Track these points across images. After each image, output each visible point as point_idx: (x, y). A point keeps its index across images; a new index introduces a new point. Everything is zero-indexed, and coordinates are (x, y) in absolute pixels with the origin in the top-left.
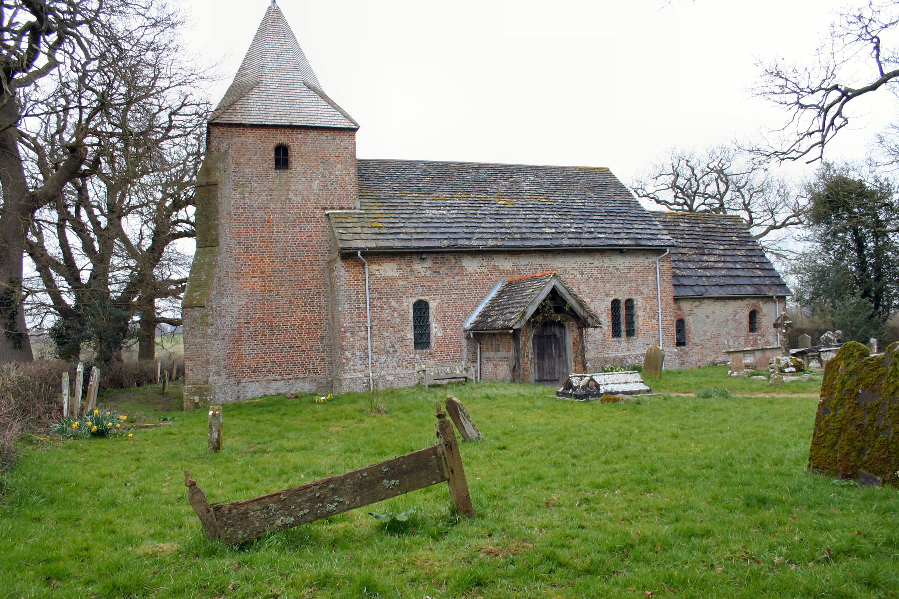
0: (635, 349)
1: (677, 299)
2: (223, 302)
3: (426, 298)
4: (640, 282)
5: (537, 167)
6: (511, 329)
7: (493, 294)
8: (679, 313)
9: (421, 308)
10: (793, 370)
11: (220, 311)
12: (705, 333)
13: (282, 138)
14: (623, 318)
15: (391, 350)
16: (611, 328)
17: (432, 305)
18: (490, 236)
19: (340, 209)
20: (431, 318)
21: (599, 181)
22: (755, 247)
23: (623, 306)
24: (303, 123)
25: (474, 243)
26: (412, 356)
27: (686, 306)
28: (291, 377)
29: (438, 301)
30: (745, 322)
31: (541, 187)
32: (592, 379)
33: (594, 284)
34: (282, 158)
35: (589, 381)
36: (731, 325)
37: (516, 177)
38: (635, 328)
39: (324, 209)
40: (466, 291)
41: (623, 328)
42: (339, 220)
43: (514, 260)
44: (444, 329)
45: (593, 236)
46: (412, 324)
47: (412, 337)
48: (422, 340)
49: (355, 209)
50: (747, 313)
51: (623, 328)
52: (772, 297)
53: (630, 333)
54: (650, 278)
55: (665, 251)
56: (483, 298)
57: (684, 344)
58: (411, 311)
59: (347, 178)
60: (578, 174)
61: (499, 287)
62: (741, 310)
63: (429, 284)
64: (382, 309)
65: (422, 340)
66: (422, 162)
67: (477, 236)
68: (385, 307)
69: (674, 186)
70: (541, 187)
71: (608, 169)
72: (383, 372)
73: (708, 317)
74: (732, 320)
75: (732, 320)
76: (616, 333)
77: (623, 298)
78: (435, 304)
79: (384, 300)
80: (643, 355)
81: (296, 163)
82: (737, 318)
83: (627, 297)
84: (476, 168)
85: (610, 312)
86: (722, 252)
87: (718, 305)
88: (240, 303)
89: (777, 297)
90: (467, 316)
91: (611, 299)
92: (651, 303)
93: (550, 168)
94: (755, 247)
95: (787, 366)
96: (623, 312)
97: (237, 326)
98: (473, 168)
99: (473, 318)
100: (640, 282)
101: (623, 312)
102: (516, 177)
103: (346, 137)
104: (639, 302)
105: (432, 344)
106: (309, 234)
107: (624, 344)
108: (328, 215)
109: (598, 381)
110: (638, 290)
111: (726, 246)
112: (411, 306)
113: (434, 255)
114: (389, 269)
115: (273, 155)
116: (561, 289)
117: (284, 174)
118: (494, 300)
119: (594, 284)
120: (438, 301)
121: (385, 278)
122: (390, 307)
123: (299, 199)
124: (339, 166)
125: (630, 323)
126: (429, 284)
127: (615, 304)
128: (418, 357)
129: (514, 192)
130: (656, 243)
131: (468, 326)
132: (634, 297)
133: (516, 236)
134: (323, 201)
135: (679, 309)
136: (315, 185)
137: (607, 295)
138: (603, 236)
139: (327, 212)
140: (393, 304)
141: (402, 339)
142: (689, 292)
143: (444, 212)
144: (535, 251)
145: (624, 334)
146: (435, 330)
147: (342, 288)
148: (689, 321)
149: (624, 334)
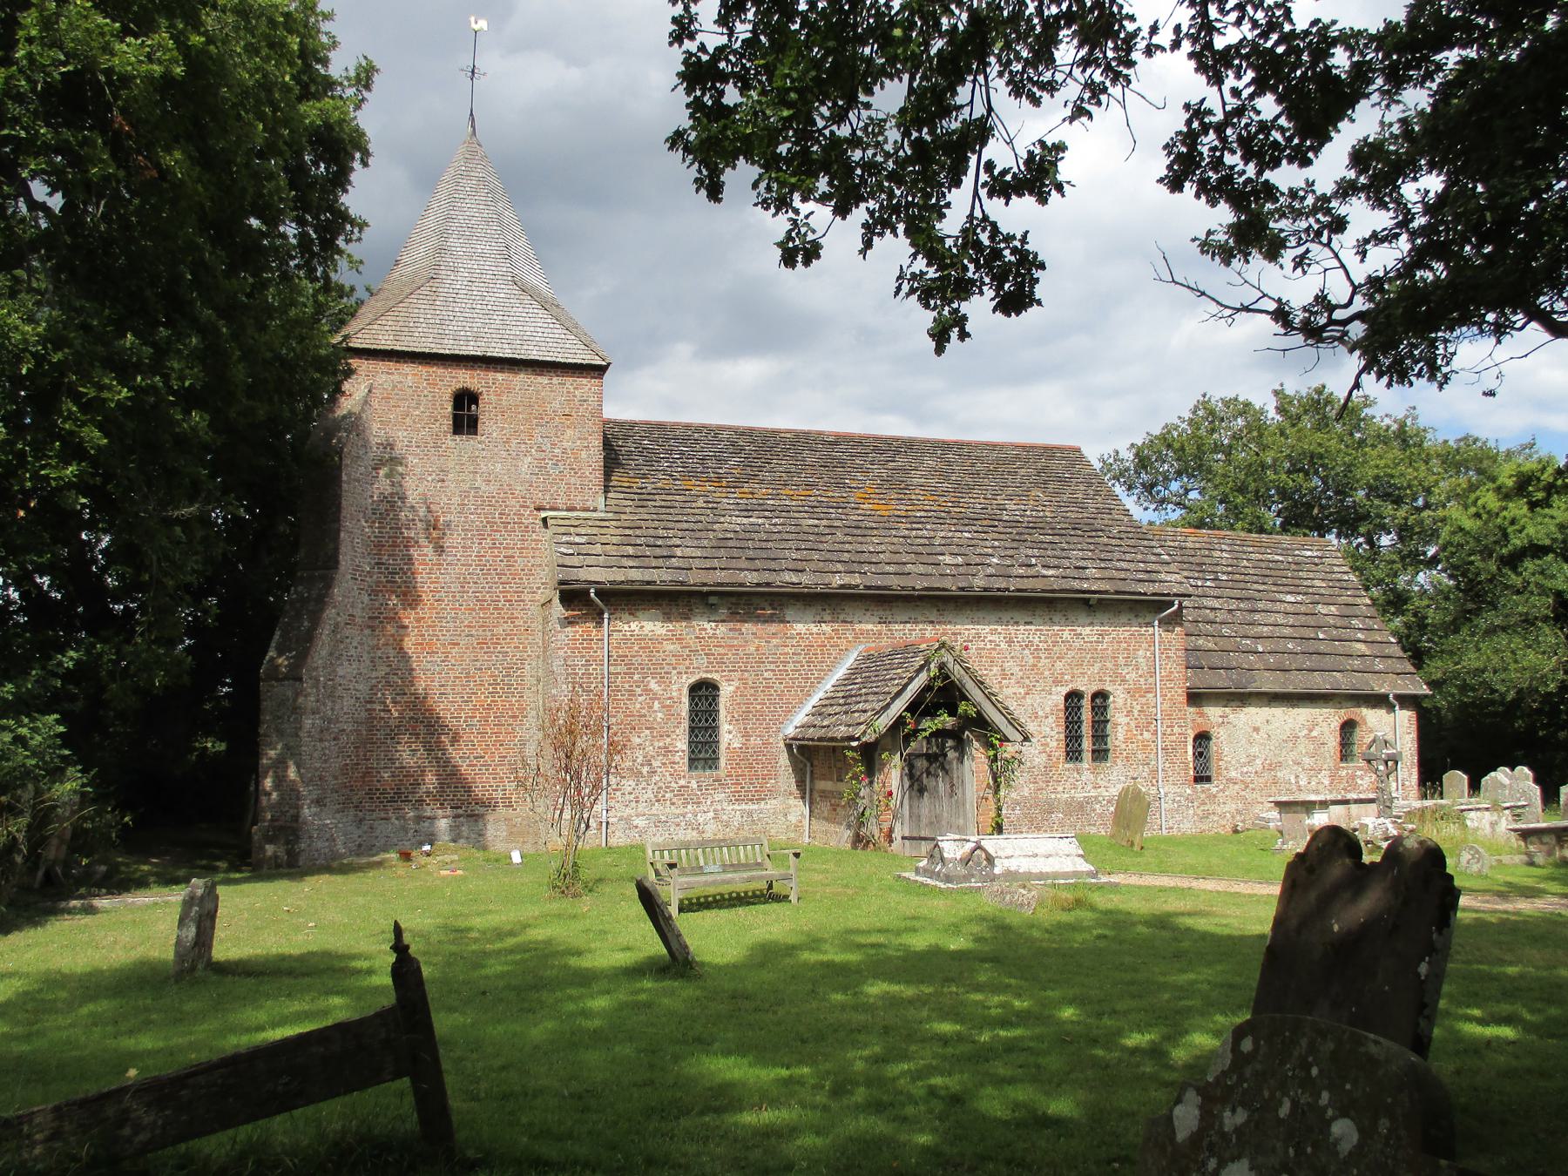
0: (1101, 785)
1: (1195, 698)
2: (340, 672)
4: (1121, 661)
5: (944, 442)
6: (858, 739)
7: (841, 672)
8: (1200, 720)
9: (703, 692)
11: (334, 687)
12: (1251, 760)
13: (466, 378)
14: (1086, 724)
15: (645, 770)
16: (1063, 744)
17: (726, 691)
18: (839, 567)
19: (568, 510)
20: (722, 713)
24: (506, 352)
25: (805, 579)
26: (682, 782)
27: (1214, 712)
28: (460, 811)
29: (736, 683)
30: (1333, 742)
32: (979, 847)
33: (1031, 661)
34: (465, 413)
38: (1110, 746)
39: (539, 509)
40: (790, 667)
41: (1087, 744)
42: (563, 530)
43: (881, 613)
44: (746, 735)
45: (1031, 572)
46: (686, 724)
47: (685, 747)
48: (703, 748)
49: (595, 510)
51: (1087, 744)
52: (1386, 697)
53: (1100, 754)
54: (1140, 653)
55: (1171, 604)
56: (820, 680)
57: (1208, 779)
58: (686, 700)
59: (584, 454)
60: (1017, 457)
61: (850, 661)
62: (1328, 720)
63: (721, 650)
64: (631, 693)
65: (703, 748)
66: (729, 428)
67: (813, 566)
68: (639, 691)
71: (1078, 450)
72: (628, 811)
73: (1256, 730)
74: (1307, 737)
75: (1307, 737)
76: (1073, 754)
77: (1088, 689)
78: (732, 688)
79: (636, 677)
81: (487, 424)
82: (1314, 734)
83: (1095, 688)
84: (830, 443)
85: (1062, 714)
86: (1290, 608)
88: (374, 674)
89: (1397, 697)
90: (789, 711)
91: (1065, 690)
92: (1143, 700)
96: (1086, 714)
97: (364, 714)
99: (800, 718)
100: (1121, 661)
101: (1086, 714)
102: (901, 461)
103: (586, 384)
104: (1118, 698)
105: (722, 762)
106: (510, 552)
107: (1087, 776)
108: (544, 520)
109: (992, 851)
110: (1118, 675)
111: (1299, 598)
112: (685, 691)
113: (733, 600)
114: (648, 627)
115: (450, 409)
116: (957, 672)
117: (465, 443)
119: (1031, 661)
120: (736, 683)
121: (640, 639)
122: (647, 691)
123: (493, 488)
124: (569, 432)
125: (1100, 735)
126: (721, 650)
127: (1073, 697)
128: (694, 784)
130: (1156, 588)
131: (790, 731)
132: (1108, 688)
133: (888, 568)
134: (540, 498)
135: (1202, 715)
136: (525, 464)
137: (1057, 682)
138: (1051, 572)
139: (543, 514)
140: (653, 685)
141: (667, 751)
142: (1220, 681)
144: (921, 598)
145: (1087, 756)
146: (728, 735)
147: (561, 653)
148: (1220, 736)
149: (1087, 756)
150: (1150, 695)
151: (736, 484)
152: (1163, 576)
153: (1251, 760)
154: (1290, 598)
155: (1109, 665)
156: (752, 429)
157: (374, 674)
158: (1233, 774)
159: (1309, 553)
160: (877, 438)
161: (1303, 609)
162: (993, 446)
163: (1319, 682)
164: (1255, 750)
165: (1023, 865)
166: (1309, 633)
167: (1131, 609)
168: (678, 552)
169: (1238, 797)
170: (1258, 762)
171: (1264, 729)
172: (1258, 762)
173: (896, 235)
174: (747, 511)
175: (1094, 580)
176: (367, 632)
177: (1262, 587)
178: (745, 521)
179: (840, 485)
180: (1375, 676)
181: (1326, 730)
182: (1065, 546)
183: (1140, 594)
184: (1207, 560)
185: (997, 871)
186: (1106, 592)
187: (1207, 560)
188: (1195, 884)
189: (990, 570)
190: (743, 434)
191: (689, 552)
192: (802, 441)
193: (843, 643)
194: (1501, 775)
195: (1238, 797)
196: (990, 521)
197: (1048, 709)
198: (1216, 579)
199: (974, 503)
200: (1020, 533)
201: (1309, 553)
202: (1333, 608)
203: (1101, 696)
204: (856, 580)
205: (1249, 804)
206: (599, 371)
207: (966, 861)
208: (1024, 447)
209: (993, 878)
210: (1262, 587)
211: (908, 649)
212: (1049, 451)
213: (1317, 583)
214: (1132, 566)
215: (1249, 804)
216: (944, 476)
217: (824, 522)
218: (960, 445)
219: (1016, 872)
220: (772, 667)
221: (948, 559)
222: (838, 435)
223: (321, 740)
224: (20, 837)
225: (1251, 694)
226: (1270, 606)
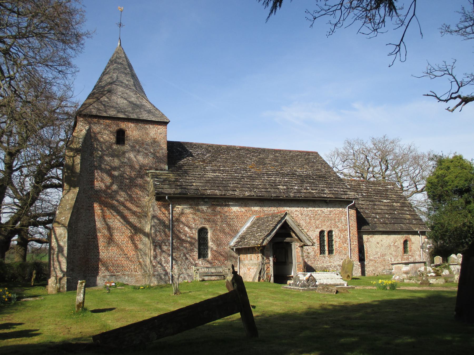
0: (336, 260)
3: (207, 226)
4: (337, 220)
7: (248, 224)
10: (434, 274)
14: (326, 242)
21: (311, 158)
22: (406, 202)
23: (326, 234)
30: (401, 247)
31: (165, 275)
32: (311, 276)
35: (309, 277)
36: (393, 248)
37: (261, 156)
45: (308, 191)
50: (402, 241)
51: (326, 248)
54: (343, 218)
60: (298, 155)
69: (355, 166)
70: (165, 275)
73: (378, 243)
75: (394, 245)
76: (322, 251)
80: (339, 265)
82: (396, 244)
83: (329, 229)
85: (319, 238)
87: (384, 236)
88: (90, 226)
91: (319, 230)
92: (344, 233)
93: (282, 150)
94: (406, 202)
95: (430, 272)
96: (326, 238)
98: (236, 150)
100: (337, 220)
101: (326, 238)
102: (261, 156)
103: (161, 129)
104: (335, 233)
107: (327, 258)
116: (290, 223)
118: (249, 228)
127: (322, 232)
129: (261, 162)
137: (317, 228)
138: (314, 191)
143: (219, 174)
150: (346, 232)
151: (210, 162)
152: (349, 193)
153: (377, 253)
154: (385, 201)
155: (333, 222)
156: (213, 145)
157: (90, 226)
158: (371, 258)
159: (389, 187)
160: (253, 148)
161: (389, 204)
162: (290, 151)
163: (397, 227)
164: (378, 250)
165: (325, 282)
166: (391, 211)
167: (339, 204)
168: (194, 184)
169: (373, 265)
170: (379, 254)
171: (380, 243)
172: (379, 254)
173: (120, 64)
174: (214, 171)
175: (327, 193)
176: (87, 211)
177: (377, 197)
178: (215, 174)
179: (243, 163)
180: (414, 225)
181: (399, 243)
182: (317, 183)
183: (342, 198)
184: (358, 189)
185: (317, 283)
186: (332, 198)
187: (358, 189)
188: (372, 288)
189: (296, 191)
190: (210, 146)
191: (198, 184)
192: (229, 149)
193: (248, 215)
194: (458, 254)
195: (373, 265)
196: (293, 174)
197: (314, 237)
198: (362, 195)
199: (287, 169)
200: (303, 179)
201: (389, 187)
202: (398, 204)
203: (330, 232)
204: (253, 193)
205: (376, 268)
206: (165, 123)
207: (308, 280)
208: (300, 152)
209: (316, 286)
210: (377, 197)
211: (273, 216)
212: (308, 153)
213: (393, 196)
214: (339, 190)
215: (376, 268)
216: (276, 161)
217: (240, 175)
218: (280, 151)
219: (323, 284)
220: (226, 223)
221: (281, 187)
222: (240, 147)
223: (73, 248)
224: (347, 208)
225: (376, 231)
226: (379, 203)
